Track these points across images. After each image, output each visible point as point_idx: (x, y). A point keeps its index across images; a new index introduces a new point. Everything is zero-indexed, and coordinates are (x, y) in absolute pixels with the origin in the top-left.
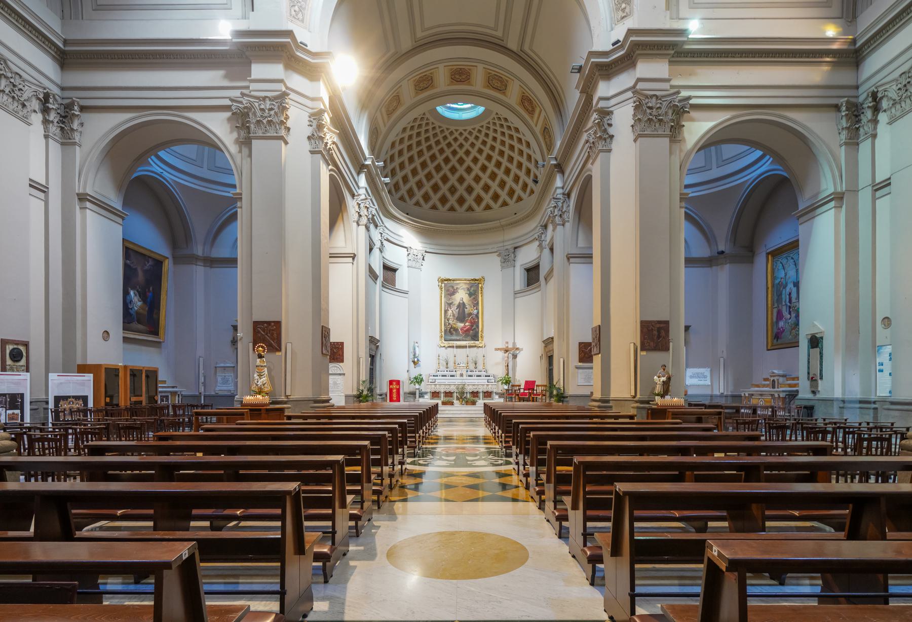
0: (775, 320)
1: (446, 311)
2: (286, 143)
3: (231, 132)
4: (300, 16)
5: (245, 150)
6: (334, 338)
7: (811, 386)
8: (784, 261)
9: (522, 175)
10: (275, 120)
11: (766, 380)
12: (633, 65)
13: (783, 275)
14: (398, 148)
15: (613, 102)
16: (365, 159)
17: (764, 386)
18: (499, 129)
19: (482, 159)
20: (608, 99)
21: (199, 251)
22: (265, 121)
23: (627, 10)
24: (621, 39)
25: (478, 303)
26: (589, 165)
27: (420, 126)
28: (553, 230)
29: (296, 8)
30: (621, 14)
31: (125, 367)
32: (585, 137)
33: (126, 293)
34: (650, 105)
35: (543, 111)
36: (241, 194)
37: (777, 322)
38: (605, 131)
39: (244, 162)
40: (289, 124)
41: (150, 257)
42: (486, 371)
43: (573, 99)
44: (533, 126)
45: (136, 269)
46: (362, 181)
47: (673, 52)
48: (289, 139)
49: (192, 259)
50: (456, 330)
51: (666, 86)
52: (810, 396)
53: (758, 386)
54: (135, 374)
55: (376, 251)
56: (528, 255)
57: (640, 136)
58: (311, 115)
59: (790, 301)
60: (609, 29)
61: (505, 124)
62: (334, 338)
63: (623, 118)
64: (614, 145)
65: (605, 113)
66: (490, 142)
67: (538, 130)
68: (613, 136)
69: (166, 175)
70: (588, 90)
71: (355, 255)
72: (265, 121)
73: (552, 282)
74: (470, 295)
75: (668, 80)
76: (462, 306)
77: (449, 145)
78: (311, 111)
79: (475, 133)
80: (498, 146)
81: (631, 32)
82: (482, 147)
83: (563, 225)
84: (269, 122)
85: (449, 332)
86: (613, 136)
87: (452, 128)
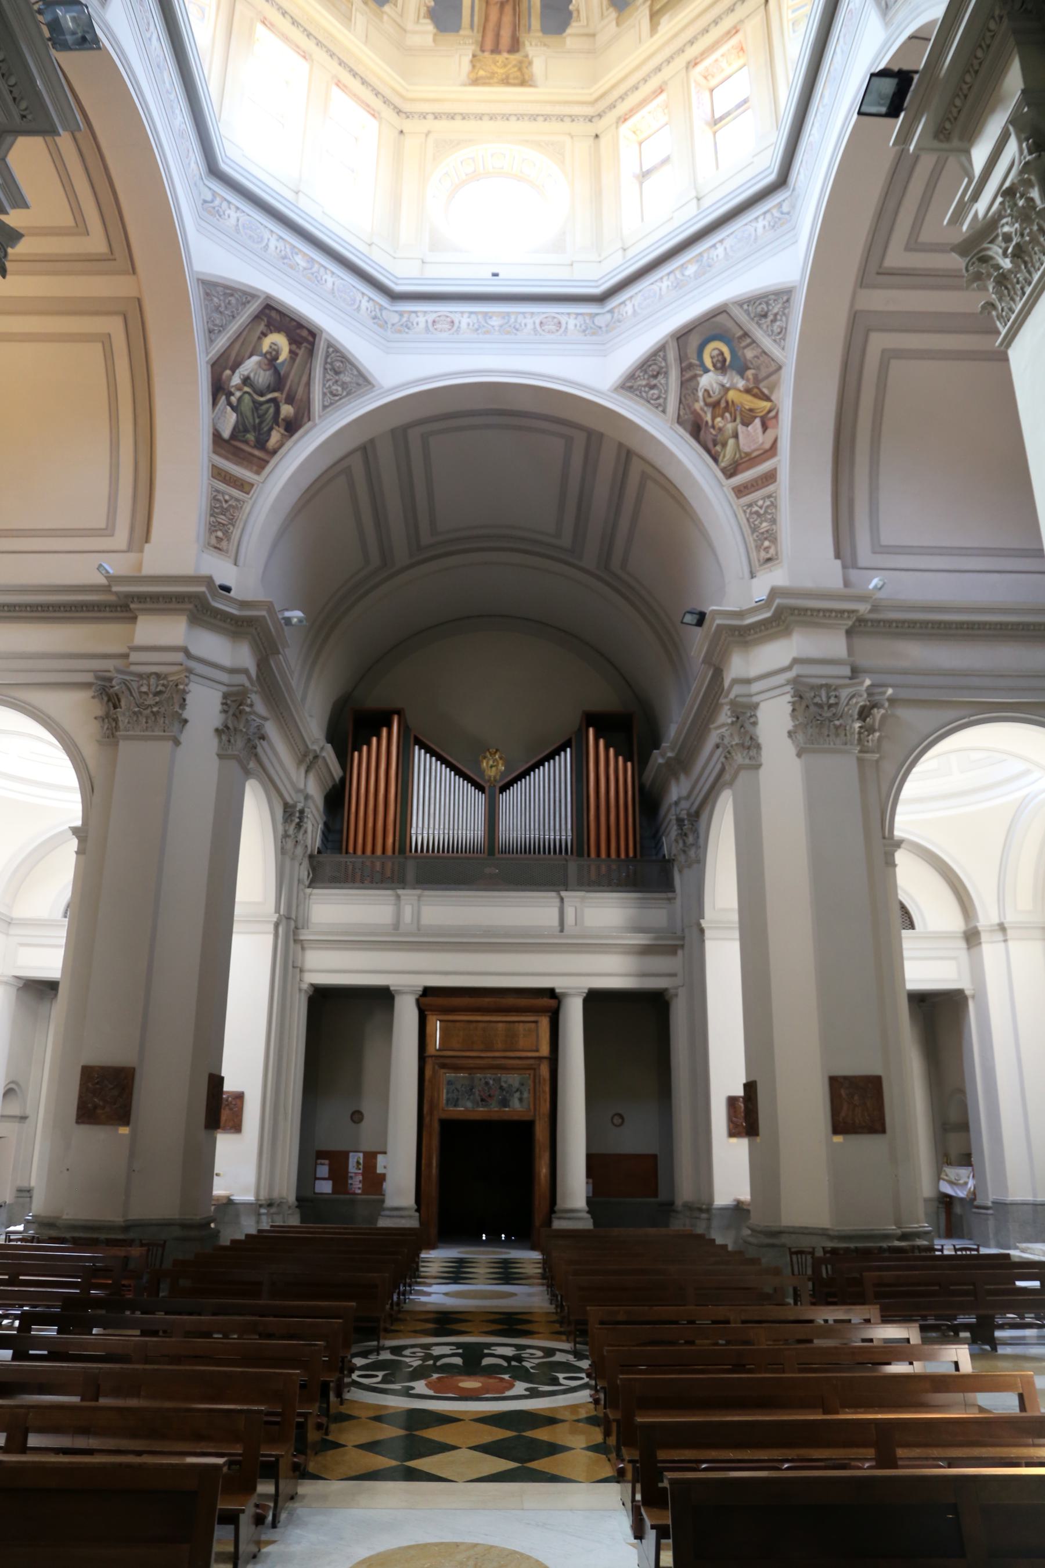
15: (755, 687)
20: (748, 681)
23: (772, 551)
30: (763, 555)
40: (186, 715)
58: (226, 696)
63: (774, 719)
64: (767, 755)
78: (225, 689)
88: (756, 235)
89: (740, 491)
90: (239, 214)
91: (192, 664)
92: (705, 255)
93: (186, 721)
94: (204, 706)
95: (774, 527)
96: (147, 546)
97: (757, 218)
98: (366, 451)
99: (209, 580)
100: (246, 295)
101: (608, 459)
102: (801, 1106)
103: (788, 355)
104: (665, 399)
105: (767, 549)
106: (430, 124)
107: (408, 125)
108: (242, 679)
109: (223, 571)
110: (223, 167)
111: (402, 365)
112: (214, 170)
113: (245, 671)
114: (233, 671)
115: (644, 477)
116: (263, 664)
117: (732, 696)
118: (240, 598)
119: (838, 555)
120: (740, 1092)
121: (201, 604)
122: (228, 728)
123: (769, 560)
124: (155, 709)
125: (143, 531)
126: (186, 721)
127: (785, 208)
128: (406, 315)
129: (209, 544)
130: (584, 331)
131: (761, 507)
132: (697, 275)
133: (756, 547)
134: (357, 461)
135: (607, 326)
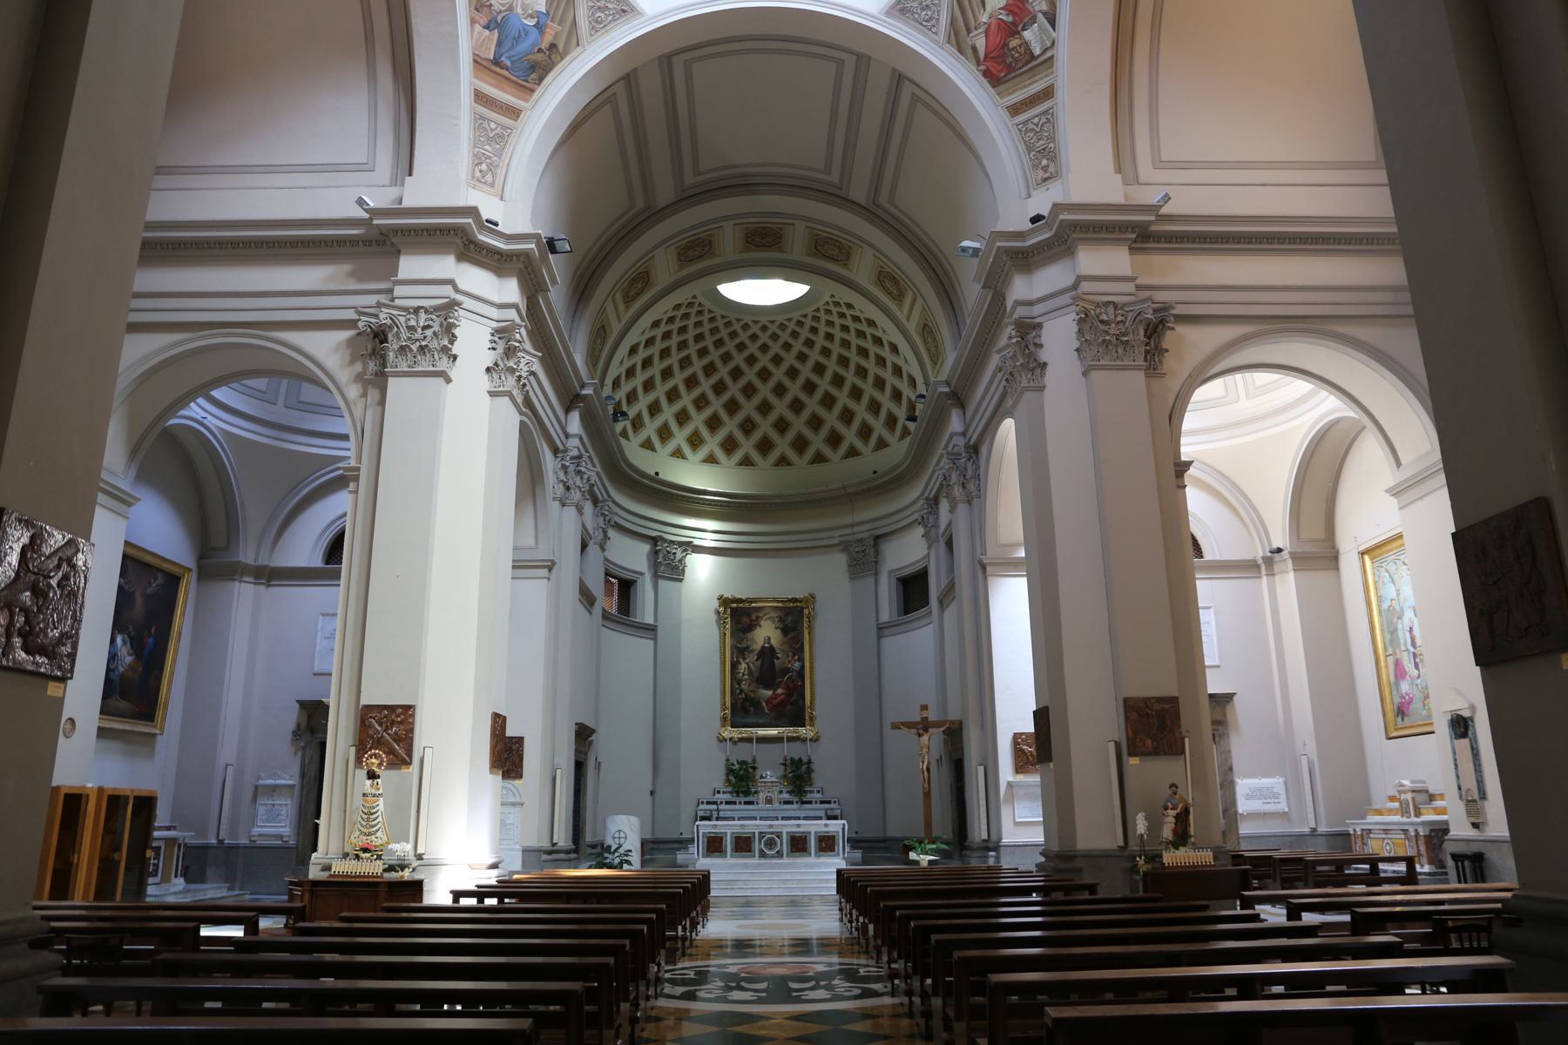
0: (1392, 679)
1: (734, 666)
2: (449, 380)
3: (352, 362)
4: (489, 178)
5: (374, 394)
6: (511, 732)
7: (1469, 813)
8: (1392, 568)
10: (434, 344)
11: (1392, 799)
13: (1394, 595)
14: (642, 354)
15: (1038, 309)
16: (583, 386)
17: (1391, 812)
18: (838, 322)
19: (806, 371)
20: (1030, 303)
21: (247, 555)
22: (414, 347)
23: (1052, 169)
24: (1045, 213)
25: (802, 649)
27: (686, 316)
29: (484, 167)
30: (1041, 174)
31: (101, 790)
32: (995, 360)
33: (113, 641)
34: (1104, 317)
35: (919, 299)
36: (358, 469)
37: (1397, 684)
38: (1031, 355)
39: (369, 413)
40: (455, 350)
41: (159, 570)
43: (972, 293)
44: (904, 321)
45: (132, 594)
46: (575, 424)
48: (452, 374)
49: (233, 572)
50: (756, 703)
52: (1471, 833)
53: (1379, 812)
54: (115, 802)
55: (593, 549)
56: (907, 552)
59: (1414, 644)
60: (1024, 195)
61: (848, 312)
62: (511, 732)
63: (1059, 339)
64: (1051, 377)
65: (1028, 330)
66: (820, 341)
67: (912, 326)
68: (1045, 364)
69: (212, 422)
71: (554, 563)
72: (414, 347)
75: (1132, 279)
76: (768, 653)
77: (741, 347)
78: (495, 325)
79: (792, 326)
80: (836, 348)
82: (803, 397)
84: (422, 348)
85: (742, 710)
86: (1045, 364)
87: (748, 319)
91: (459, 297)
93: (455, 357)
94: (474, 343)
98: (629, 80)
99: (473, 212)
101: (878, 86)
102: (1094, 731)
105: (1045, 169)
108: (512, 314)
109: (489, 208)
115: (915, 99)
117: (1016, 316)
119: (1119, 170)
120: (1030, 728)
126: (455, 357)
134: (620, 89)
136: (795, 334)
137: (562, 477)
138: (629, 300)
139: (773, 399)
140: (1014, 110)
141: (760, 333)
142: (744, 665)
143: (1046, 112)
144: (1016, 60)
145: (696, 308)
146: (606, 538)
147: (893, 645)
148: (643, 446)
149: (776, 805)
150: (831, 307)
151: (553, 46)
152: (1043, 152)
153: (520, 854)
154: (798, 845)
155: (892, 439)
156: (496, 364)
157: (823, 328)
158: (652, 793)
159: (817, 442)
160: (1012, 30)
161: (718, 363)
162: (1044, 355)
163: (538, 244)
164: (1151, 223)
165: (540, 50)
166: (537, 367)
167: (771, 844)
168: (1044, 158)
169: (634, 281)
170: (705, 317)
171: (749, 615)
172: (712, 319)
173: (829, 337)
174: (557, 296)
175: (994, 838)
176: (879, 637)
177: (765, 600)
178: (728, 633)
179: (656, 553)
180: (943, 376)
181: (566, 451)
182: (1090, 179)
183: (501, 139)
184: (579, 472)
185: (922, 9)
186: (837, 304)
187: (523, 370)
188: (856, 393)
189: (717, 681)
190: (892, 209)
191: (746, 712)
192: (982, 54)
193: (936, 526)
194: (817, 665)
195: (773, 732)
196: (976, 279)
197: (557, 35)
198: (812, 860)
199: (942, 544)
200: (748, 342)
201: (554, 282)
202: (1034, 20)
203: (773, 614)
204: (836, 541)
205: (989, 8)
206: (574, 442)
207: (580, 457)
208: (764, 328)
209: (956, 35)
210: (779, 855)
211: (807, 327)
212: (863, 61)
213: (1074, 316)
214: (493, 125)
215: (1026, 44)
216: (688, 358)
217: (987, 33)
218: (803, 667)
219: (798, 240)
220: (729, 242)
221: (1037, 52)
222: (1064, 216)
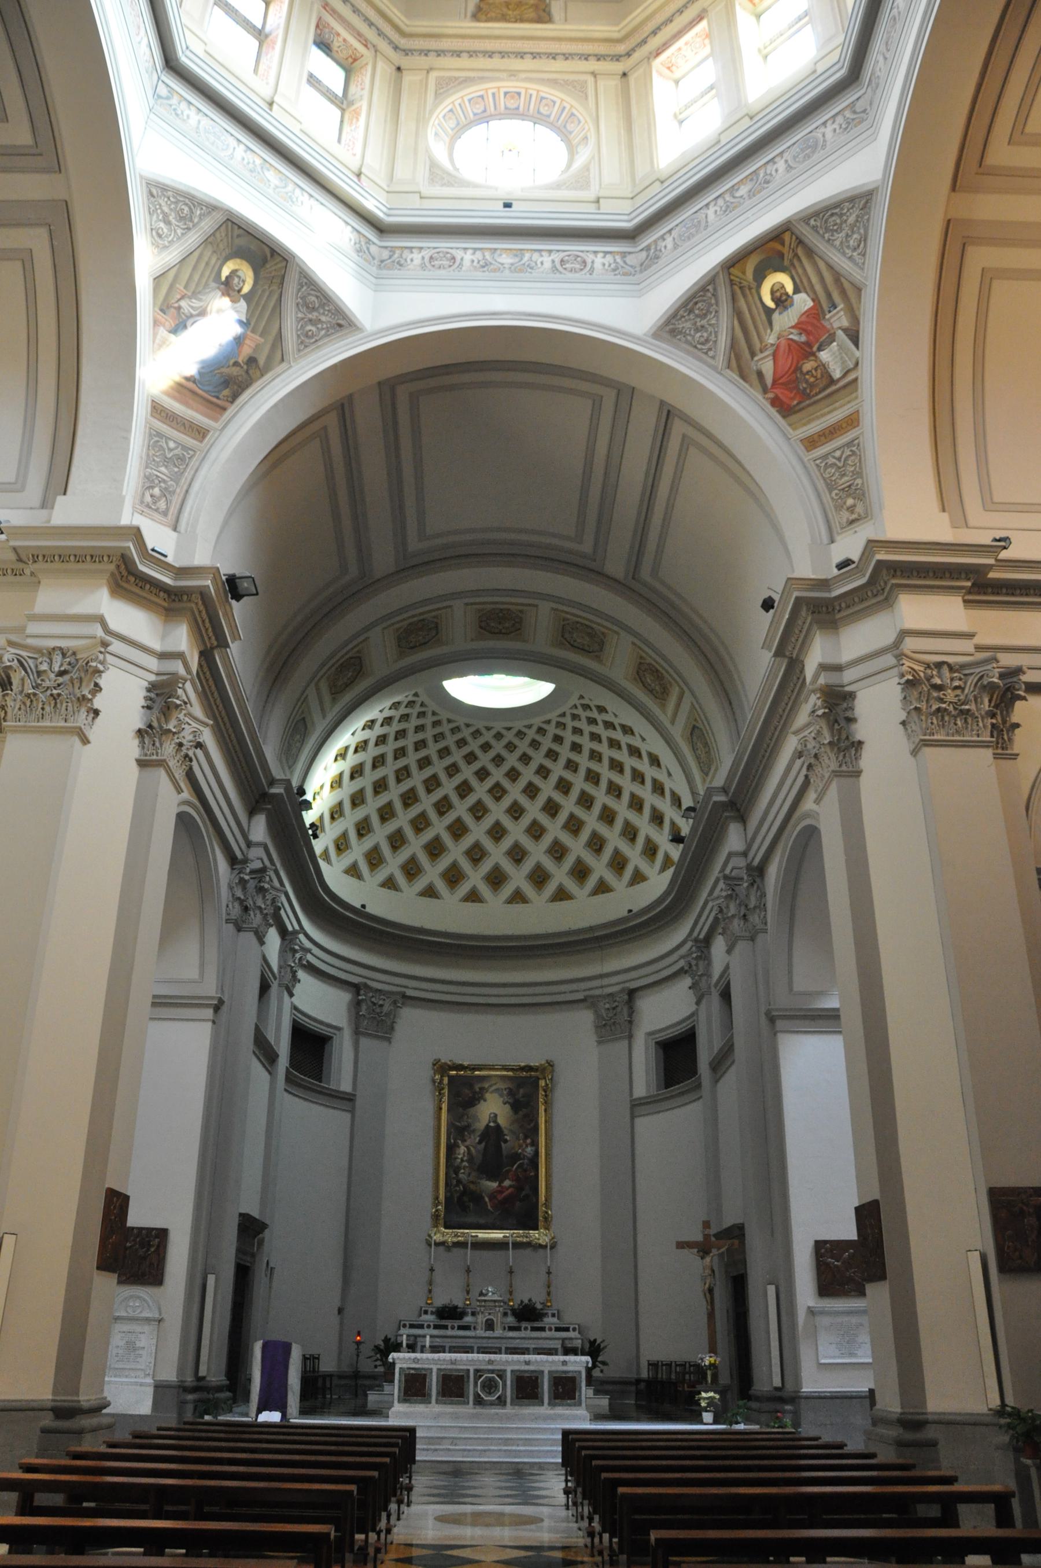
1: (451, 1149)
2: (85, 741)
4: (162, 504)
6: (137, 1218)
9: (645, 793)
12: (887, 602)
15: (848, 676)
23: (860, 509)
24: (855, 557)
25: (536, 1129)
26: (809, 804)
28: (729, 951)
29: (156, 491)
30: (846, 515)
32: (790, 745)
35: (687, 694)
40: (98, 703)
42: (558, 1315)
43: (757, 668)
44: (668, 725)
46: (259, 829)
47: (969, 584)
50: (477, 1198)
51: (967, 646)
56: (664, 1010)
57: (926, 743)
58: (152, 687)
60: (826, 540)
62: (137, 1218)
64: (868, 760)
65: (838, 704)
67: (677, 732)
70: (789, 651)
73: (731, 1078)
74: (516, 1106)
75: (970, 636)
76: (493, 1134)
78: (153, 678)
79: (531, 734)
81: (872, 545)
83: (752, 939)
85: (459, 1206)
86: (860, 743)
88: (824, 141)
89: (811, 443)
90: (200, 116)
92: (762, 173)
93: (96, 713)
94: (122, 697)
95: (859, 481)
96: (60, 499)
97: (824, 124)
98: (343, 409)
100: (212, 208)
103: (871, 274)
104: (715, 342)
105: (851, 509)
106: (432, 60)
107: (404, 62)
109: (159, 537)
110: (184, 59)
111: (388, 307)
112: (171, 64)
113: (180, 656)
114: (163, 656)
116: (206, 656)
118: (177, 565)
120: (848, 1231)
121: (129, 574)
122: (150, 726)
123: (853, 522)
124: (55, 692)
125: (59, 480)
126: (96, 713)
127: (859, 107)
128: (398, 252)
129: (142, 502)
130: (614, 270)
131: (839, 459)
132: (752, 194)
133: (836, 507)
134: (332, 421)
135: (642, 265)
136: (535, 744)
137: (239, 893)
138: (336, 692)
139: (507, 822)
140: (811, 443)
141: (493, 742)
142: (462, 1149)
143: (850, 444)
144: (812, 386)
145: (418, 709)
146: (295, 979)
147: (648, 1126)
148: (347, 872)
149: (498, 1332)
150: (580, 711)
151: (252, 361)
152: (849, 490)
153: (150, 1390)
154: (527, 1388)
155: (651, 871)
156: (150, 726)
157: (569, 737)
158: (340, 1311)
159: (560, 875)
160: (806, 351)
161: (443, 777)
162: (861, 731)
163: (214, 580)
164: (990, 567)
165: (236, 364)
166: (207, 737)
167: (490, 1386)
168: (847, 491)
169: (343, 667)
170: (428, 720)
171: (471, 1086)
172: (436, 724)
173: (576, 747)
174: (241, 658)
175: (789, 1386)
176: (633, 1117)
177: (492, 1068)
178: (445, 1106)
179: (359, 1003)
180: (719, 781)
181: (245, 861)
182: (909, 513)
183: (180, 461)
184: (261, 890)
185: (697, 330)
186: (586, 707)
187: (187, 736)
188: (608, 816)
189: (429, 1169)
190: (658, 586)
191: (455, 1094)
192: (769, 381)
193: (708, 974)
194: (556, 1151)
195: (497, 1235)
196: (766, 646)
197: (257, 348)
198: (544, 1410)
199: (715, 999)
200: (478, 752)
201: (236, 637)
202: (832, 338)
203: (502, 1085)
204: (580, 996)
205: (777, 327)
206: (256, 853)
207: (263, 870)
208: (499, 736)
209: (738, 358)
210: (501, 1402)
211: (550, 735)
212: (626, 395)
213: (897, 680)
214: (172, 445)
215: (823, 367)
216: (406, 769)
217: (775, 355)
218: (537, 1153)
219: (542, 623)
220: (459, 623)
221: (837, 374)
222: (882, 556)
